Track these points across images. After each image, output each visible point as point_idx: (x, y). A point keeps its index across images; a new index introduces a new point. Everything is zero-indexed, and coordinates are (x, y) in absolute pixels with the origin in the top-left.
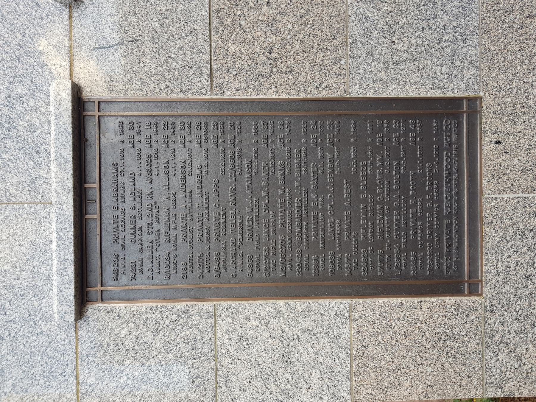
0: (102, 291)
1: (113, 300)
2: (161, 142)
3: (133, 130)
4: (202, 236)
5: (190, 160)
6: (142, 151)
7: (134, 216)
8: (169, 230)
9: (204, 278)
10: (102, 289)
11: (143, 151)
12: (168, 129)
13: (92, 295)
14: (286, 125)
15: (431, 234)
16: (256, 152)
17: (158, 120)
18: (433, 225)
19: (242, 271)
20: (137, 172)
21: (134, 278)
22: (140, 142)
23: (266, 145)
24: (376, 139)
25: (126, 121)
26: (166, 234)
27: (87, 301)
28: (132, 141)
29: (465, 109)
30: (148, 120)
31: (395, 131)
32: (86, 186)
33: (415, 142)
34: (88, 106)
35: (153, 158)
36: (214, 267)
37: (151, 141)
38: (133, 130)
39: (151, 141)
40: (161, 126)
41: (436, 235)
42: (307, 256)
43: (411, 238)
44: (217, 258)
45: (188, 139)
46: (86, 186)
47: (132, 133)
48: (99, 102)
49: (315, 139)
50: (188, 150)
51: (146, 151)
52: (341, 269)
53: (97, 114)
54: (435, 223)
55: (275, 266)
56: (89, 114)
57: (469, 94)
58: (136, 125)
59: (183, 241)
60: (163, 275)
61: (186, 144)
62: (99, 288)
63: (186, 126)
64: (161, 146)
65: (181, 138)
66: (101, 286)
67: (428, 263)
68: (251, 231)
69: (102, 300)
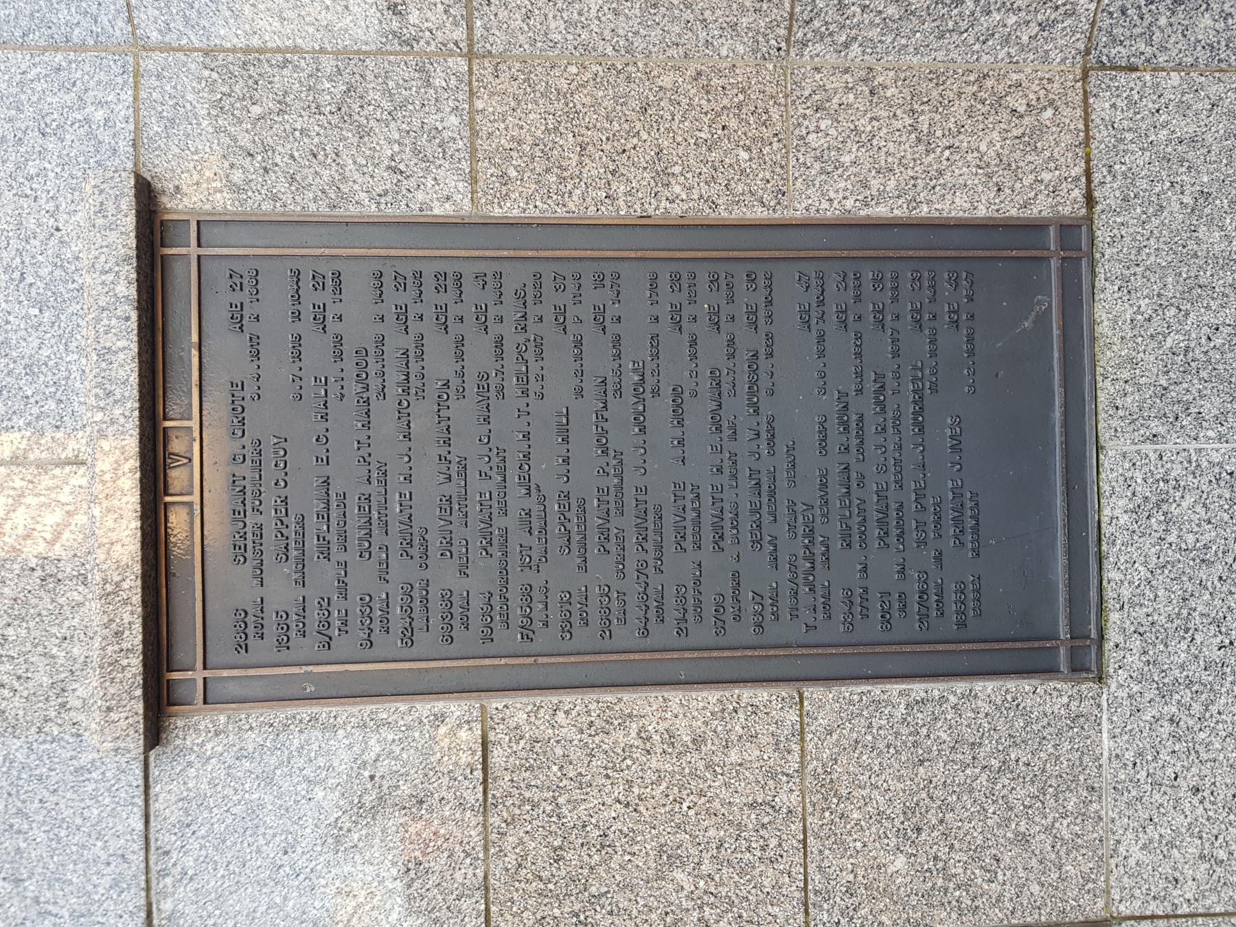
4: (410, 544)
5: (380, 365)
7: (367, 496)
9: (689, 636)
10: (207, 674)
12: (241, 289)
13: (180, 692)
17: (731, 267)
21: (646, 632)
27: (171, 703)
36: (516, 614)
37: (242, 316)
39: (242, 316)
42: (384, 596)
44: (405, 597)
47: (676, 298)
51: (748, 341)
55: (345, 623)
61: (721, 324)
62: (198, 675)
64: (428, 327)
65: (399, 310)
66: (205, 668)
69: (205, 702)
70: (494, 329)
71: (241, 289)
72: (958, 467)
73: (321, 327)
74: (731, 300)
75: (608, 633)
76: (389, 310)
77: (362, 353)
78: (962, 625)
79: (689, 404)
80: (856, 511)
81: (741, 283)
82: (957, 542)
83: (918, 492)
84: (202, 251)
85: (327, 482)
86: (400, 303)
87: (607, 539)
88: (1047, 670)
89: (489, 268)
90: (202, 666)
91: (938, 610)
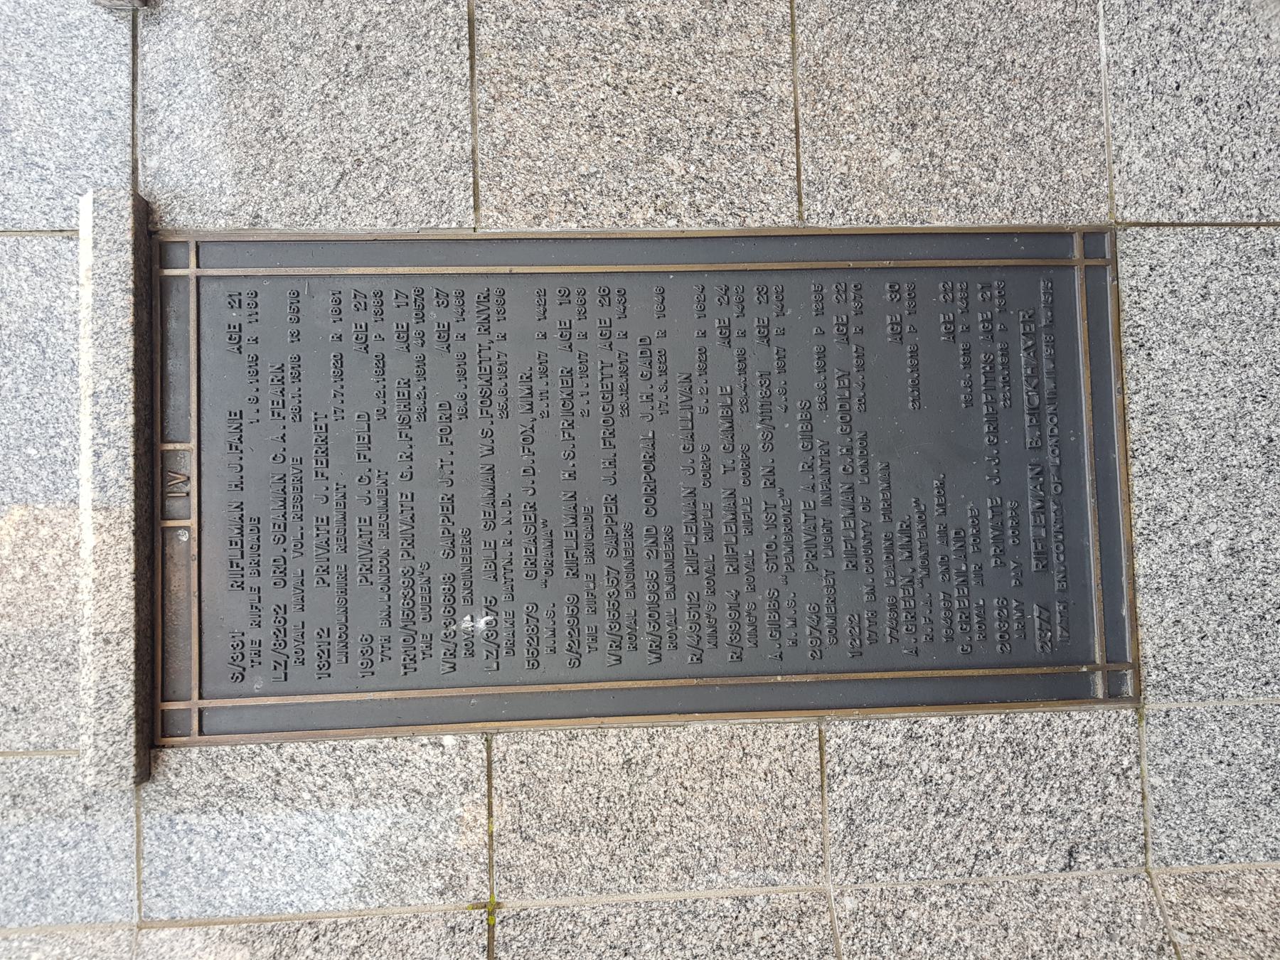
0: (201, 712)
2: (595, 336)
8: (242, 557)
10: (205, 703)
14: (852, 295)
19: (795, 643)
21: (535, 664)
24: (977, 323)
35: (577, 376)
37: (240, 337)
39: (240, 337)
40: (593, 298)
45: (578, 327)
53: (192, 271)
57: (1099, 214)
58: (615, 298)
59: (364, 580)
60: (564, 655)
62: (195, 703)
63: (452, 300)
64: (392, 346)
74: (583, 315)
76: (552, 325)
82: (811, 567)
84: (202, 272)
85: (240, 507)
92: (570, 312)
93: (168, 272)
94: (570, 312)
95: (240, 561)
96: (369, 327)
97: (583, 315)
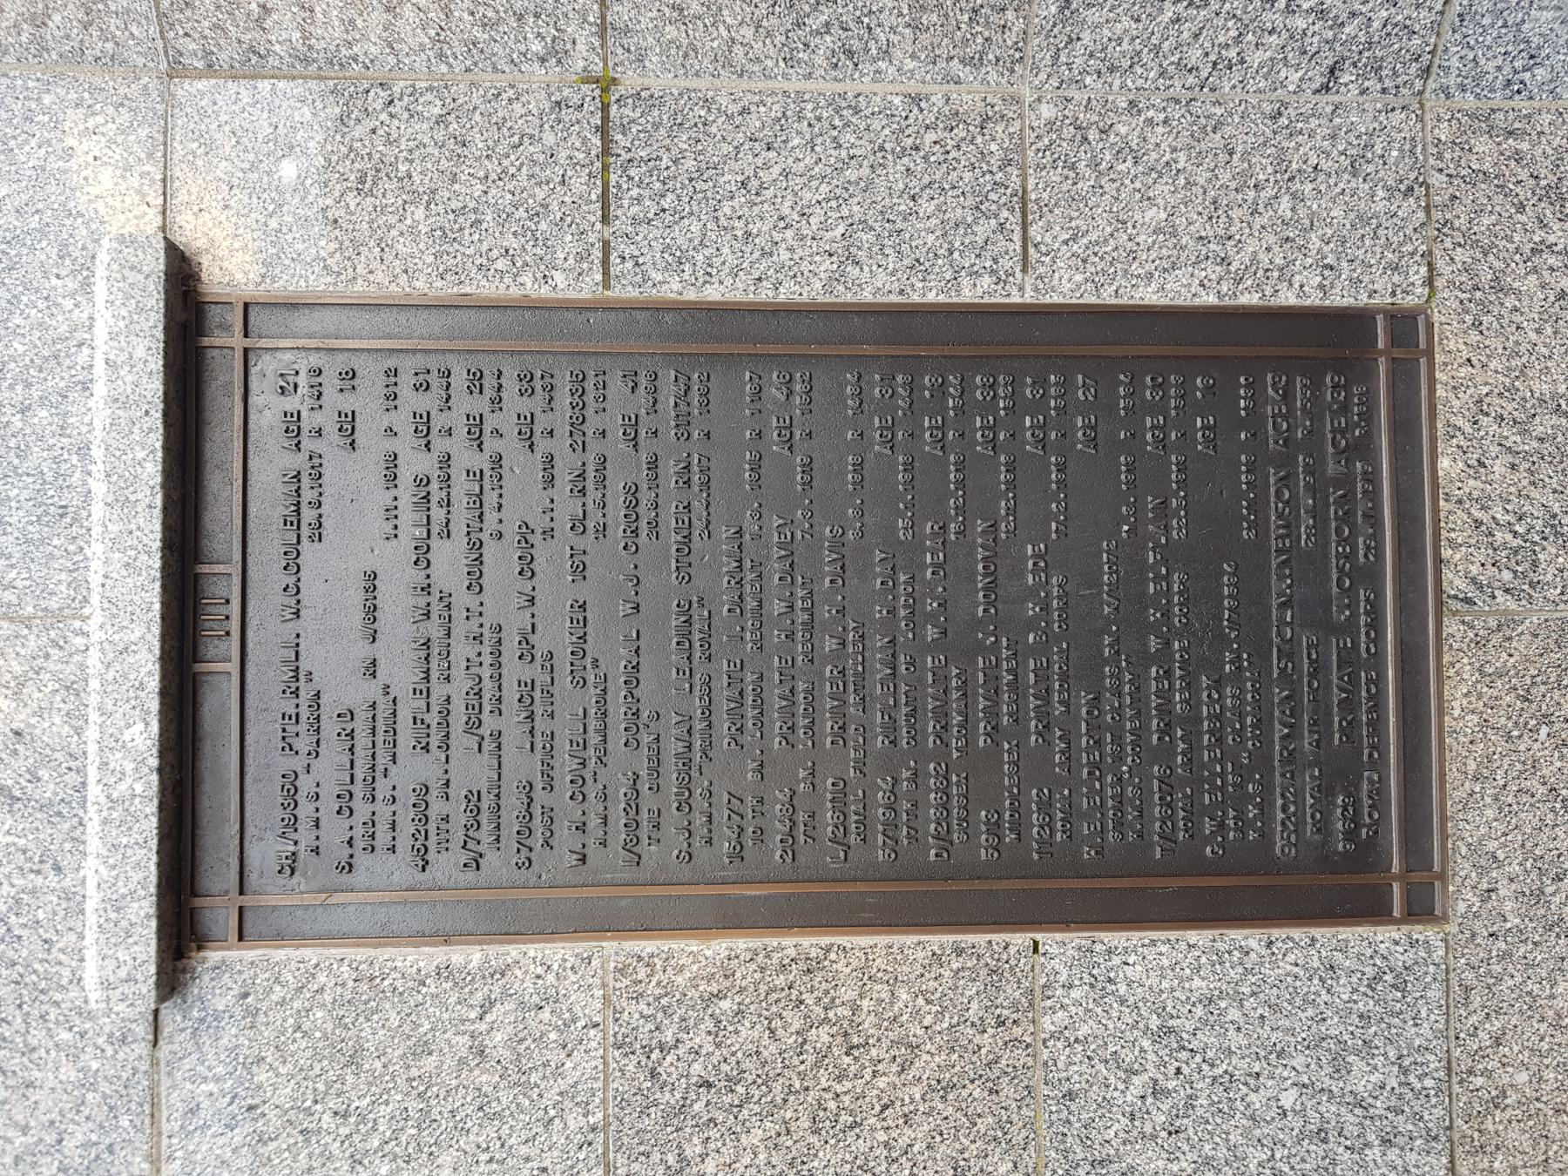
1: (280, 937)
3: (530, 396)
5: (444, 494)
6: (608, 465)
11: (558, 462)
12: (481, 392)
15: (1167, 729)
16: (859, 467)
17: (605, 364)
18: (1170, 701)
20: (539, 522)
22: (319, 432)
23: (475, 444)
25: (407, 365)
26: (419, 725)
28: (477, 430)
29: (1381, 345)
30: (420, 361)
31: (1153, 410)
32: (205, 569)
33: (1162, 443)
34: (214, 315)
38: (530, 396)
39: (299, 428)
41: (1179, 733)
43: (931, 745)
45: (438, 422)
46: (205, 569)
47: (481, 404)
48: (246, 305)
49: (937, 428)
50: (311, 458)
52: (864, 840)
54: (1178, 698)
56: (218, 342)
63: (538, 384)
64: (511, 446)
67: (1035, 822)
68: (840, 713)
69: (241, 938)
70: (542, 445)
71: (481, 392)
72: (993, 639)
73: (527, 444)
75: (790, 853)
77: (423, 482)
78: (738, 854)
79: (541, 551)
80: (903, 699)
81: (511, 386)
83: (1040, 673)
84: (248, 343)
86: (289, 408)
87: (792, 728)
88: (1372, 909)
89: (434, 363)
90: (237, 890)
91: (1186, 831)
92: (481, 404)
93: (206, 341)
94: (428, 402)
95: (426, 716)
96: (536, 421)
97: (497, 402)
